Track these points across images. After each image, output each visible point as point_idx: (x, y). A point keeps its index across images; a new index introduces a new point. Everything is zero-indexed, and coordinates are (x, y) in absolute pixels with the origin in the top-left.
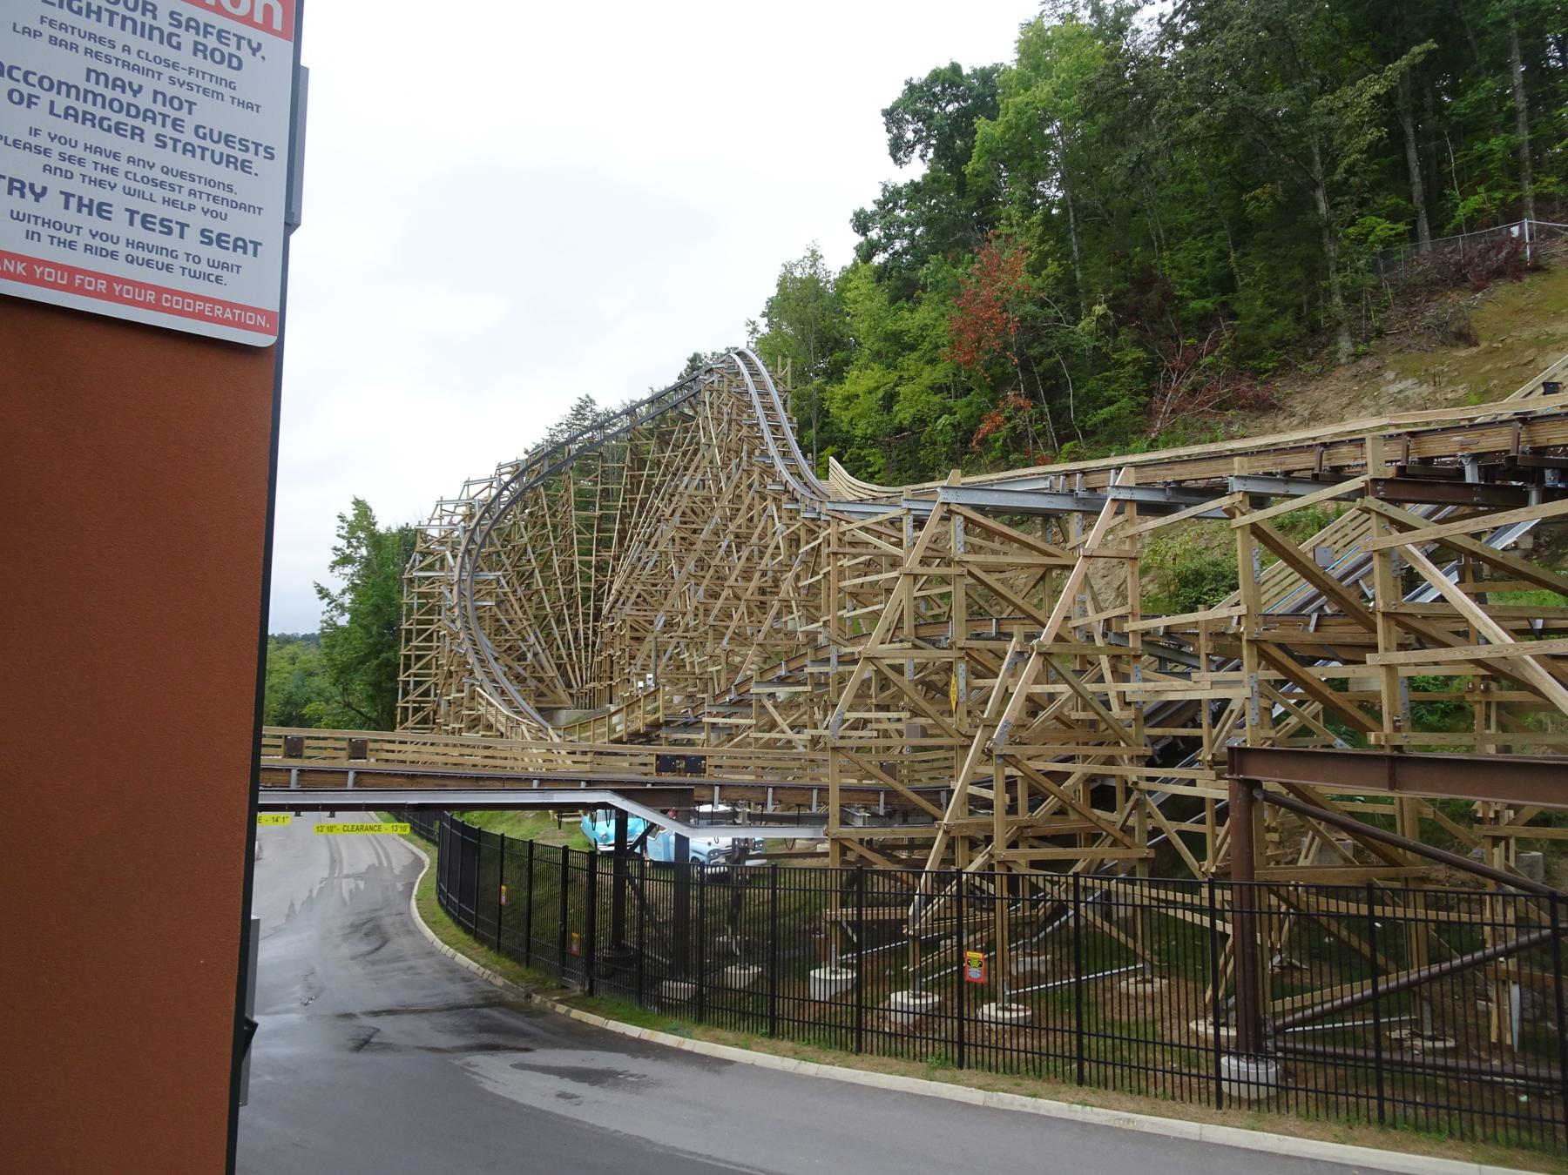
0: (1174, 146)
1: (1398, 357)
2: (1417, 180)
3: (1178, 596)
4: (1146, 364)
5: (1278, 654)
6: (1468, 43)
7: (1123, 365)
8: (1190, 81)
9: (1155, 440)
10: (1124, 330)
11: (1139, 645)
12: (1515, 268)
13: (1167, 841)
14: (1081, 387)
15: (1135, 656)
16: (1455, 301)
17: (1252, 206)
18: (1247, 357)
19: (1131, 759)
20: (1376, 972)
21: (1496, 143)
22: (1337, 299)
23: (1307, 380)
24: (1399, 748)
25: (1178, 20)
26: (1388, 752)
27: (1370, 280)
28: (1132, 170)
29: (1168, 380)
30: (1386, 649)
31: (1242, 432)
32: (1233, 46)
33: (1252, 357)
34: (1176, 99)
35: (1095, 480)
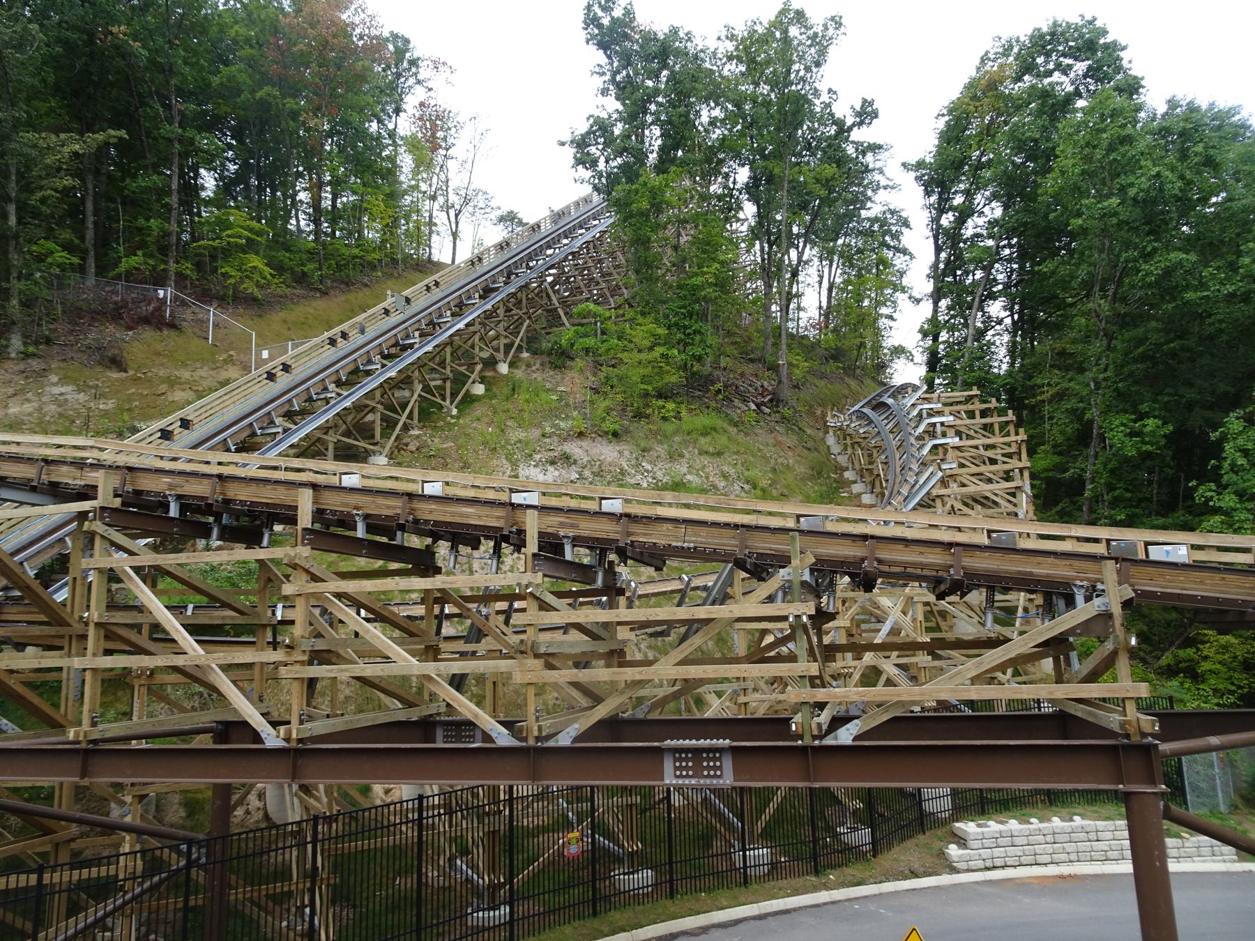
1: (62, 365)
2: (91, 226)
12: (156, 320)
16: (111, 332)
22: (15, 302)
26: (83, 746)
30: (94, 655)
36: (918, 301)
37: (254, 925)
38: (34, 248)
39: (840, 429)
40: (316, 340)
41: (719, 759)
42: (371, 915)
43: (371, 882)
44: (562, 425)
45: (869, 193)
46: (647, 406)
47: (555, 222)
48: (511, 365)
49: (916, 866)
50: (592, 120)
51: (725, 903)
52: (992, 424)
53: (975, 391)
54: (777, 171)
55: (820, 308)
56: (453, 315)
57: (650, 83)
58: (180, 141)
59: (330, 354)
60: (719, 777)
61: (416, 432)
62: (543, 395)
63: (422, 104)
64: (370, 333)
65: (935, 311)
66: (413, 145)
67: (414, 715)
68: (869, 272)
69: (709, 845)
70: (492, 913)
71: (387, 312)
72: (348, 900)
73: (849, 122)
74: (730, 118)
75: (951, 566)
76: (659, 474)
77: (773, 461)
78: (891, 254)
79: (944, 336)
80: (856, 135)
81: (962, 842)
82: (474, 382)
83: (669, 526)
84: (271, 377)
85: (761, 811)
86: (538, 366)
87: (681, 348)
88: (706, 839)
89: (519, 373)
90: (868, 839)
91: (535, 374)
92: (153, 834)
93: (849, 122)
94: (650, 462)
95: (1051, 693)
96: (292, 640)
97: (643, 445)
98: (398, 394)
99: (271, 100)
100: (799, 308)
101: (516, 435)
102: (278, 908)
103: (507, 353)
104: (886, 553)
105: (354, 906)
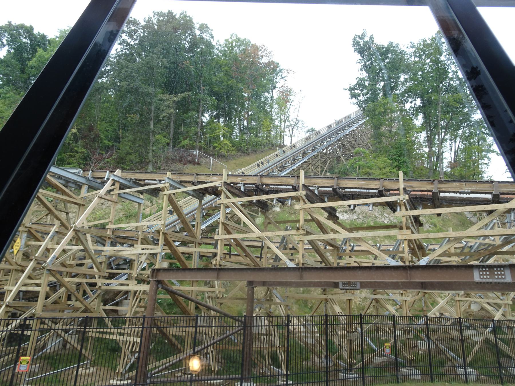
12: (193, 162)
47: (337, 125)
60: (504, 279)
64: (271, 164)
71: (277, 156)
74: (411, 79)
76: (392, 219)
94: (387, 214)
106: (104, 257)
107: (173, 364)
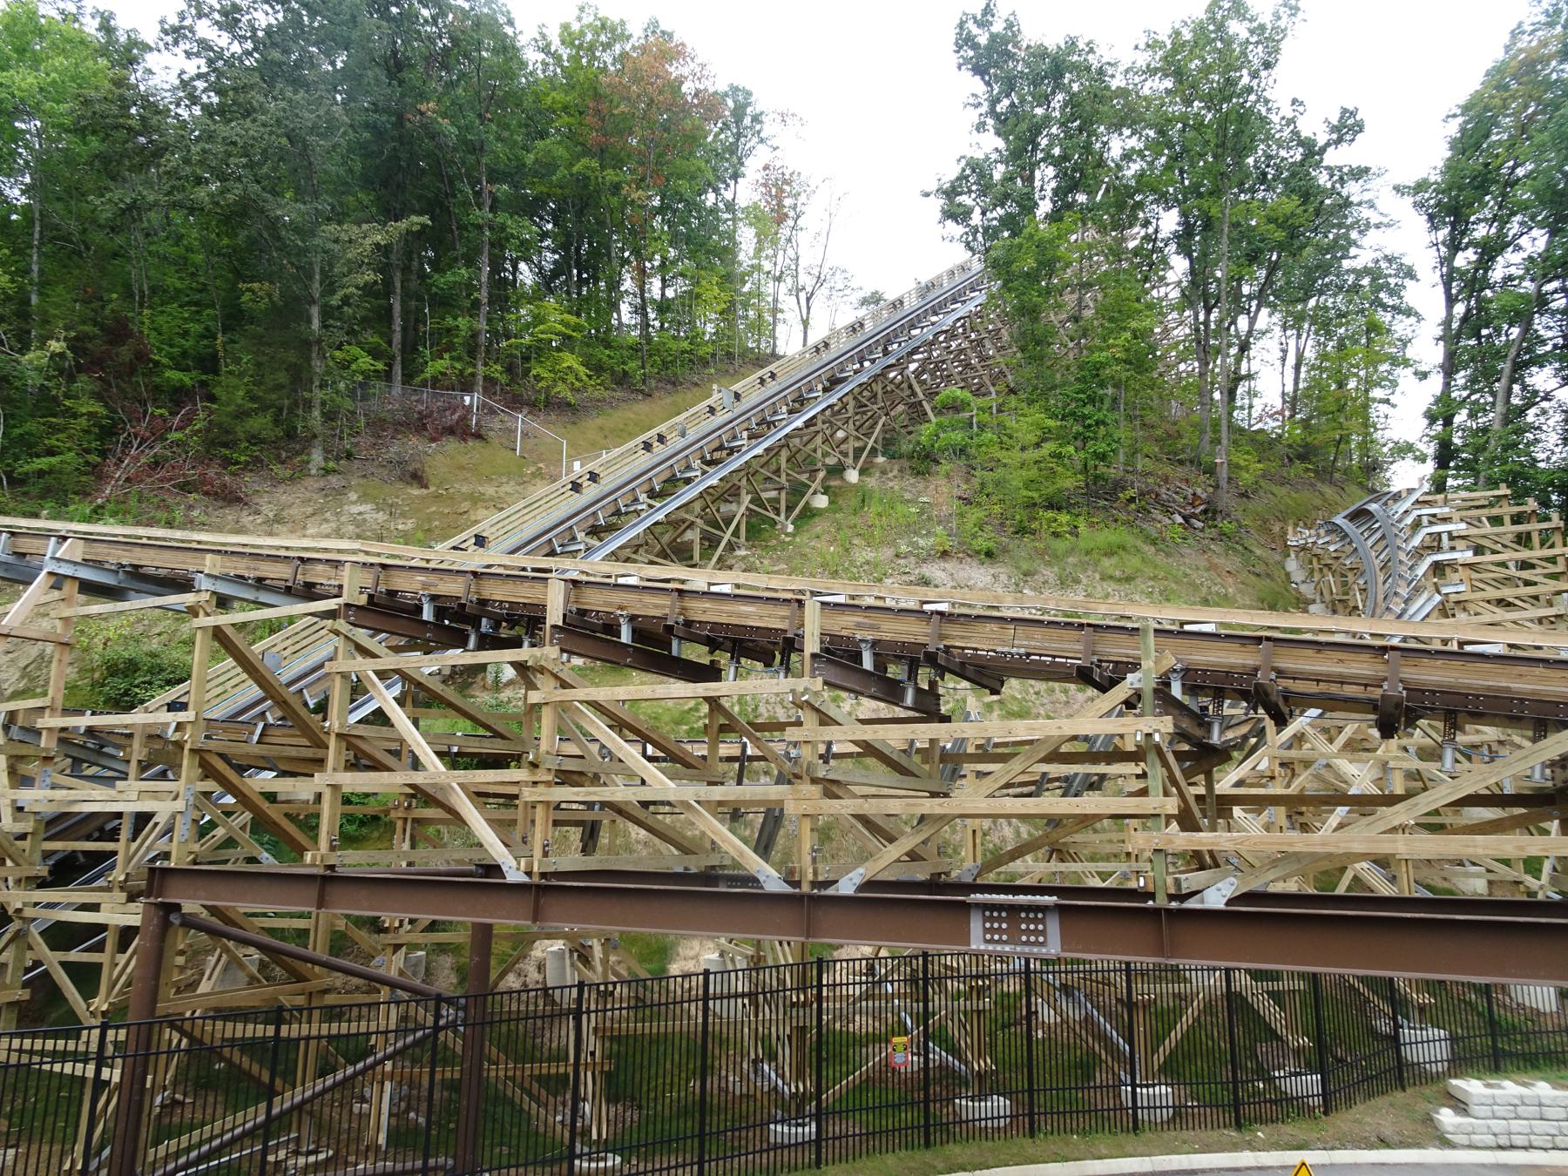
0: (174, 205)
1: (362, 481)
3: (103, 685)
4: (104, 422)
5: (220, 765)
6: (452, 231)
7: (75, 416)
8: (204, 151)
9: (102, 507)
10: (83, 377)
11: (53, 745)
12: (462, 431)
13: (46, 974)
14: (15, 426)
15: (46, 758)
16: (413, 446)
17: (247, 297)
18: (219, 444)
19: (18, 882)
20: (270, 1093)
21: (462, 322)
22: (316, 413)
23: (278, 482)
24: (332, 867)
25: (197, 83)
26: (321, 871)
27: (348, 404)
28: (123, 211)
29: (127, 445)
30: (335, 770)
31: (203, 518)
32: (254, 138)
33: (225, 445)
34: (187, 161)
35: (25, 545)
36: (1423, 376)
37: (525, 1116)
38: (337, 353)
39: (1304, 548)
40: (631, 444)
41: (1042, 921)
42: (659, 1119)
43: (660, 1081)
44: (922, 542)
45: (1354, 235)
46: (1032, 519)
47: (923, 297)
48: (862, 472)
49: (1387, 1132)
50: (963, 162)
51: (1105, 1152)
52: (1529, 534)
53: (1504, 490)
54: (1214, 211)
55: (1283, 394)
56: (790, 412)
57: (1039, 111)
58: (491, 228)
59: (644, 460)
60: (1042, 944)
61: (742, 552)
62: (900, 507)
63: (766, 168)
64: (691, 437)
65: (1447, 385)
66: (754, 216)
67: (695, 865)
68: (1356, 342)
69: (1089, 1076)
70: (800, 1130)
71: (712, 410)
72: (633, 1099)
73: (1321, 141)
74: (1155, 147)
75: (1385, 679)
77: (1204, 590)
78: (1389, 315)
79: (1461, 417)
80: (1332, 157)
81: (1460, 1105)
82: (815, 493)
83: (994, 627)
84: (576, 487)
85: (1160, 1040)
86: (895, 472)
87: (1079, 443)
88: (1086, 1068)
89: (872, 482)
90: (1317, 1089)
91: (891, 482)
92: (404, 988)
93: (1321, 141)
95: (1521, 848)
96: (537, 755)
97: (1025, 566)
98: (724, 508)
99: (589, 173)
100: (1252, 394)
101: (863, 554)
102: (551, 1099)
103: (856, 458)
104: (1290, 661)
105: (640, 1107)
106: (32, 818)
107: (255, 1127)
